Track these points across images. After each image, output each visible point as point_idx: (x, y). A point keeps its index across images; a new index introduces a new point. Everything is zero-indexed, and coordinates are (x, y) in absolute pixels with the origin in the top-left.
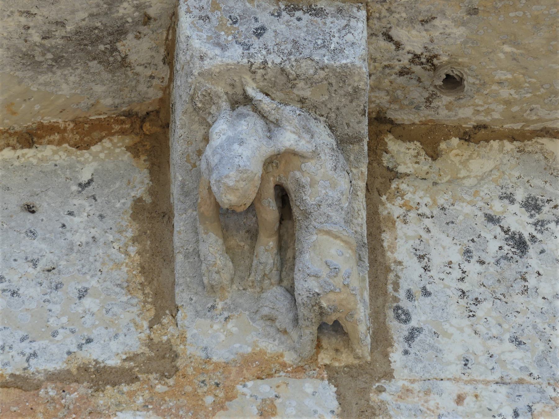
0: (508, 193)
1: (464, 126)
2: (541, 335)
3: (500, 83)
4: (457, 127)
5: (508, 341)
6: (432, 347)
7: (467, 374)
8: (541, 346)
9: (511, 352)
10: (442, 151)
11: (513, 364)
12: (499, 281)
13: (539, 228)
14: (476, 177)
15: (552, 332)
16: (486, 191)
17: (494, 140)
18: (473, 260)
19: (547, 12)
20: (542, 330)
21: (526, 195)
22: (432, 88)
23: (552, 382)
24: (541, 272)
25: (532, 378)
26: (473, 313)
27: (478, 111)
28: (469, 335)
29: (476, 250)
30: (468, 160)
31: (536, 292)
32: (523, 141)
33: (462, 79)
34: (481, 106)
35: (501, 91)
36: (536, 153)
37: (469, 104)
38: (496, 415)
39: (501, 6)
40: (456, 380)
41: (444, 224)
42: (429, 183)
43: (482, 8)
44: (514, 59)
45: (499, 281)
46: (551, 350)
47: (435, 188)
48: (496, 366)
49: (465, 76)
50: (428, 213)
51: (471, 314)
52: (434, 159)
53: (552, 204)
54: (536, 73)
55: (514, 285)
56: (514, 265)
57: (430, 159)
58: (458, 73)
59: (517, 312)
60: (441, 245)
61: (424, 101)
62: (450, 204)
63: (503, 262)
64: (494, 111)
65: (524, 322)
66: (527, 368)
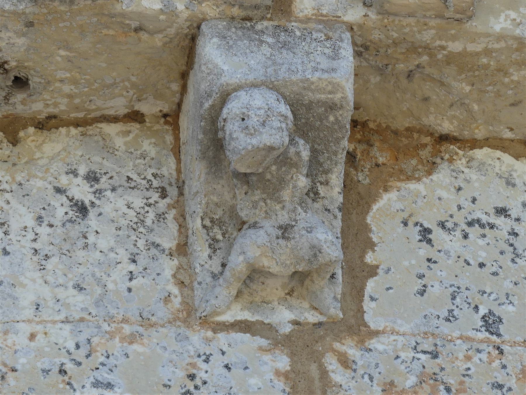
0: (73, 169)
1: (38, 117)
2: (98, 281)
3: (61, 81)
4: (32, 119)
5: (71, 288)
6: (10, 296)
7: (38, 316)
8: (99, 290)
9: (74, 296)
10: (21, 138)
11: (75, 306)
12: (65, 240)
13: (97, 195)
14: (48, 157)
15: (107, 279)
16: (55, 168)
17: (62, 127)
18: (44, 225)
19: (89, 21)
20: (99, 277)
21: (87, 170)
22: (6, 89)
23: (107, 319)
24: (99, 231)
25: (91, 316)
26: (43, 267)
27: (48, 104)
28: (40, 285)
29: (47, 216)
30: (41, 144)
31: (95, 247)
32: (85, 127)
33: (27, 79)
34: (50, 100)
35: (63, 87)
36: (96, 135)
37: (40, 99)
38: (61, 348)
39: (51, 18)
40: (29, 321)
41: (21, 197)
42: (9, 164)
43: (37, 21)
44: (69, 61)
45: (65, 240)
46: (106, 293)
47: (14, 168)
48: (61, 308)
49: (30, 77)
50: (8, 188)
51: (42, 267)
52: (14, 145)
53: (108, 176)
54: (89, 71)
55: (77, 242)
56: (77, 227)
57: (11, 145)
58: (24, 75)
59: (79, 264)
60: (19, 214)
61: (3, 98)
62: (26, 180)
63: (68, 225)
64: (60, 103)
65: (84, 272)
66: (86, 309)
